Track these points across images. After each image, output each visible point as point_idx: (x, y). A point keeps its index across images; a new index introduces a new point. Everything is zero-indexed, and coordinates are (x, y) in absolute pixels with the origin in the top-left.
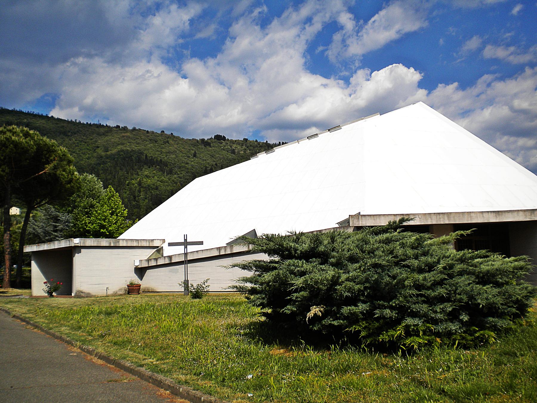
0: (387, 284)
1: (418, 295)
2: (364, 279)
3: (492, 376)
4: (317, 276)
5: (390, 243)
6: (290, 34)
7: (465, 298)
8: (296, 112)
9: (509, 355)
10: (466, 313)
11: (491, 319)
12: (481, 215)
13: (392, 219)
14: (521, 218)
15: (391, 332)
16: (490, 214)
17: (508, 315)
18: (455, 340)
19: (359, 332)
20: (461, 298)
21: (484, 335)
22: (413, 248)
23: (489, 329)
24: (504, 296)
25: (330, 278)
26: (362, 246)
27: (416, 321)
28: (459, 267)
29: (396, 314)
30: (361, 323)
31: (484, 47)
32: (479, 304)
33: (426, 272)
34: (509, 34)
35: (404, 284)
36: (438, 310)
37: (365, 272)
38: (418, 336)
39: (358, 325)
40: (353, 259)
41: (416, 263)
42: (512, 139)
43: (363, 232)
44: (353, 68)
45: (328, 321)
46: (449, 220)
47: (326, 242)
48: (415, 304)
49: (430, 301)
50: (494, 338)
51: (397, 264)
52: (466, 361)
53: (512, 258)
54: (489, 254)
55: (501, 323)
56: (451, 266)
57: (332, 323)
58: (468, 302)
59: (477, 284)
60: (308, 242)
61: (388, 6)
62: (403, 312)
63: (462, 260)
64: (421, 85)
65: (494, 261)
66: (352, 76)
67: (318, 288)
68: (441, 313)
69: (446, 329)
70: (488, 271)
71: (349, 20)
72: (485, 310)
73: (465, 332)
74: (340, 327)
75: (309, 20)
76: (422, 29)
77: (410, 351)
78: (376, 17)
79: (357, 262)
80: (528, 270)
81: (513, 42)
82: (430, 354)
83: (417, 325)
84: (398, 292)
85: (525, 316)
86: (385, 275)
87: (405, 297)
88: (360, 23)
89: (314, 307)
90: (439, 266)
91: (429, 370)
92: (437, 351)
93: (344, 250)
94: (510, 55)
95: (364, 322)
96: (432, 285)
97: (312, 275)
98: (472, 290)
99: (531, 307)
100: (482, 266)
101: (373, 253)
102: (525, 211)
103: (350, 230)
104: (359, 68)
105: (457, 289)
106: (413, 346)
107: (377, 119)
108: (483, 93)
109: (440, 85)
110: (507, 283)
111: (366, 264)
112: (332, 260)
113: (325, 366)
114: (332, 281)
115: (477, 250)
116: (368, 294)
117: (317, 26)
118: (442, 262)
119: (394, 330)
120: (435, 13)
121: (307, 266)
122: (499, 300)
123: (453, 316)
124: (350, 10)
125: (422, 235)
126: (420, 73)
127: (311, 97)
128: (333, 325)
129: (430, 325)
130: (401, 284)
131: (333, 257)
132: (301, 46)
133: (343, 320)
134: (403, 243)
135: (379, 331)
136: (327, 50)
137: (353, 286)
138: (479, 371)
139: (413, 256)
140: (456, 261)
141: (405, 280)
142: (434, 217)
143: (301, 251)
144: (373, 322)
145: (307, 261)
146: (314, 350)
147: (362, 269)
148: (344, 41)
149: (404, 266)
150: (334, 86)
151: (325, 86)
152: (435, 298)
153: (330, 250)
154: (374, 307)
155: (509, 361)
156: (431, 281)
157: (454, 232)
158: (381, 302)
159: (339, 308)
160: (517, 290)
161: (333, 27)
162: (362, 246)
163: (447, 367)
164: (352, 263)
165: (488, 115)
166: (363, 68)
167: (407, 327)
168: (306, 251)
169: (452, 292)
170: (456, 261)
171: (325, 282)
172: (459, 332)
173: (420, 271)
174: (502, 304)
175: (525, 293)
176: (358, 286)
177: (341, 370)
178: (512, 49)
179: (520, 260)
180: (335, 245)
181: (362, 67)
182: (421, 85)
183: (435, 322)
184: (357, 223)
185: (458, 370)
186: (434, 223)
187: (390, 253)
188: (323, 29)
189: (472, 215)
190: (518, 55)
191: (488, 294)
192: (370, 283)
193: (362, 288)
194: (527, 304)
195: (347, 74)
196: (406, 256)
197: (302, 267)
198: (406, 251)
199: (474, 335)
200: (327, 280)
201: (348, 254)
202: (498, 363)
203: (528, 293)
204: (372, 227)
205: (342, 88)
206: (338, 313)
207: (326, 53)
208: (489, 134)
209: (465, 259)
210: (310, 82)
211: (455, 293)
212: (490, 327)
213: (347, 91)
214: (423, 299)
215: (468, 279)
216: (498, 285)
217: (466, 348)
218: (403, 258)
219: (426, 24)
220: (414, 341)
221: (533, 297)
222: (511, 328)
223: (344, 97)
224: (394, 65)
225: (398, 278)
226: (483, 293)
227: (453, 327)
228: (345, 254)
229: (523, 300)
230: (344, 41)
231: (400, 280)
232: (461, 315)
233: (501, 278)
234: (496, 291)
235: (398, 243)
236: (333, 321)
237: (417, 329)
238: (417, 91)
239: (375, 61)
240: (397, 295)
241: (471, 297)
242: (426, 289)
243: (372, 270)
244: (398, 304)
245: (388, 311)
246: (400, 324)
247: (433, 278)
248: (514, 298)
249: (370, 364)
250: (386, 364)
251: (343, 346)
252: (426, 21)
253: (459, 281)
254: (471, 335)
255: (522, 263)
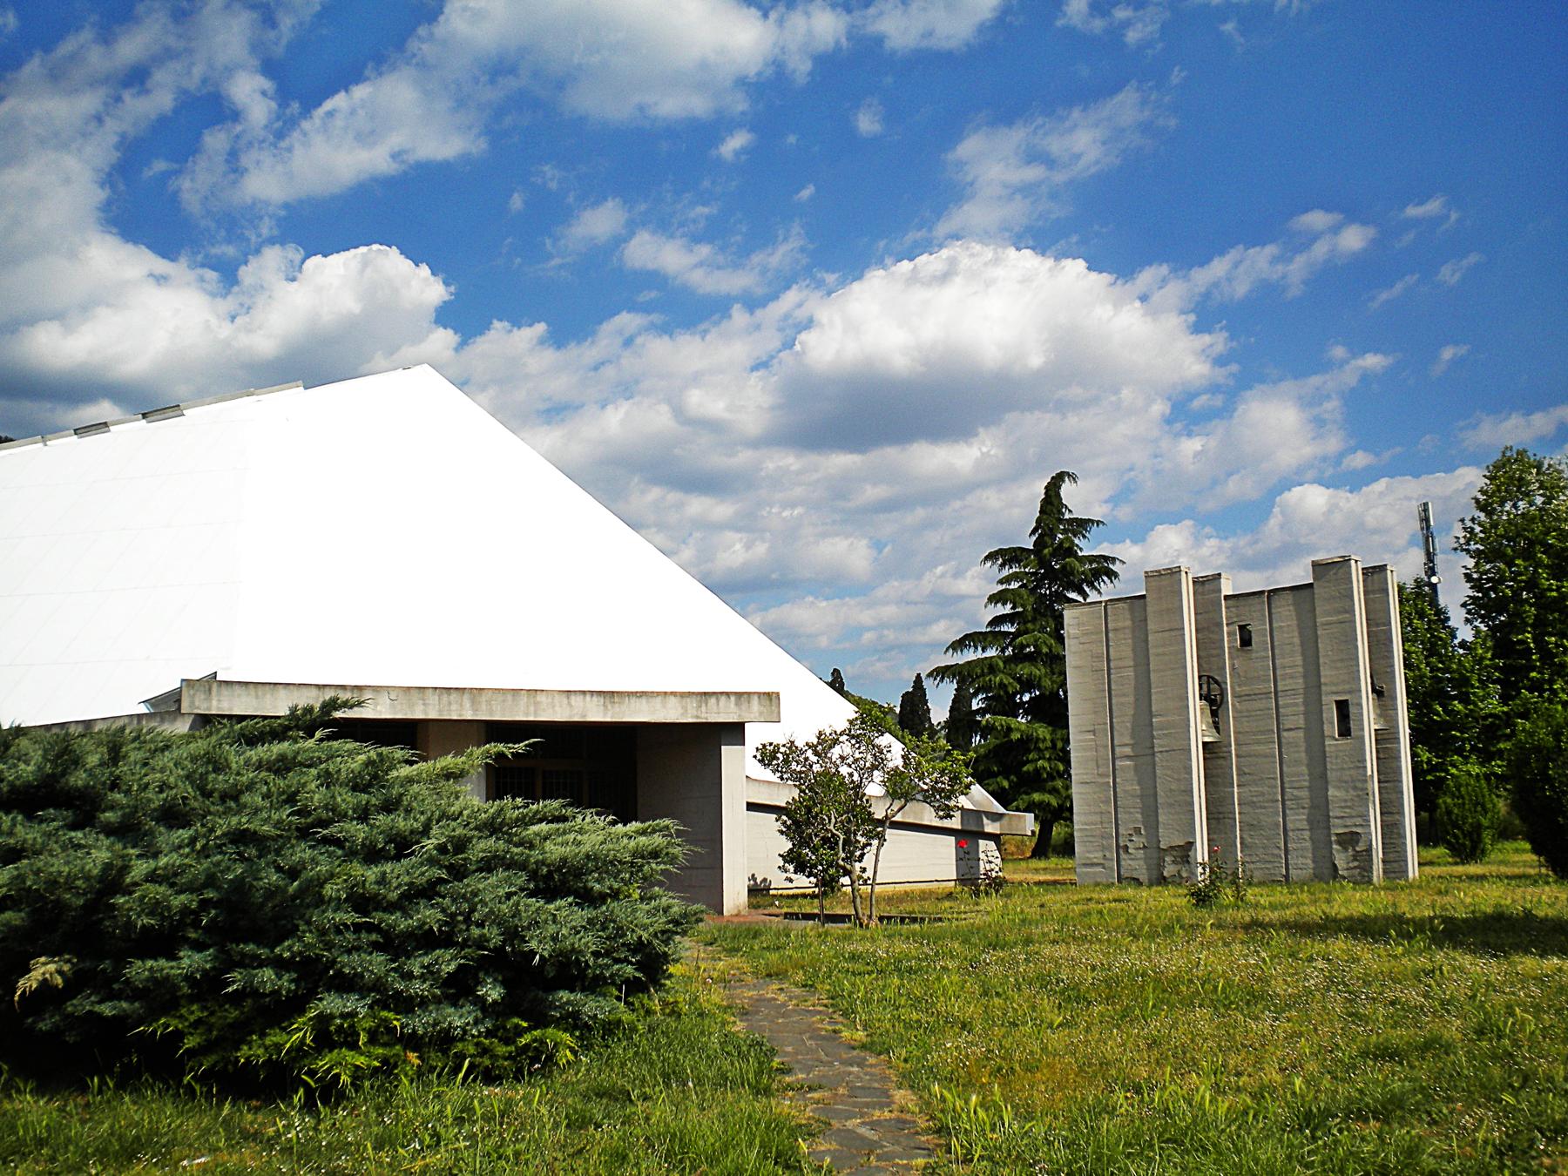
0: (271, 893)
1: (358, 928)
2: (202, 878)
3: (556, 1159)
4: (58, 865)
5: (289, 770)
6: (64, 108)
7: (494, 936)
8: (57, 347)
9: (610, 1097)
10: (495, 980)
11: (564, 995)
12: (565, 701)
13: (304, 700)
14: (596, 713)
15: (274, 1037)
16: (588, 697)
17: (613, 983)
18: (461, 1057)
19: (178, 1036)
20: (483, 935)
21: (542, 1042)
22: (356, 788)
23: (558, 1023)
24: (603, 930)
25: (95, 872)
26: (203, 776)
27: (351, 1003)
28: (483, 846)
29: (291, 981)
30: (183, 1011)
31: (632, 234)
32: (533, 953)
33: (388, 859)
34: (706, 210)
35: (320, 894)
36: (417, 971)
37: (207, 857)
38: (353, 1046)
39: (175, 1017)
40: (173, 816)
41: (358, 832)
42: (673, 496)
43: (211, 734)
44: (253, 238)
45: (82, 1004)
46: (475, 711)
47: (93, 760)
48: (349, 952)
49: (395, 946)
50: (572, 1050)
51: (304, 833)
52: (488, 1118)
53: (634, 826)
54: (569, 811)
55: (593, 1007)
56: (461, 845)
57: (97, 1008)
58: (503, 947)
59: (530, 896)
60: (37, 756)
61: (380, 74)
62: (315, 975)
63: (493, 827)
64: (444, 316)
65: (581, 831)
66: (246, 263)
67: (58, 901)
68: (423, 978)
69: (435, 1024)
70: (564, 860)
71: (258, 97)
72: (551, 972)
73: (490, 1034)
74: (121, 1022)
75: (137, 78)
76: (465, 158)
77: (329, 1093)
78: (339, 101)
79: (186, 824)
80: (673, 859)
81: (711, 233)
82: (387, 1101)
83: (353, 1014)
84: (302, 917)
85: (660, 987)
86: (268, 865)
87: (323, 932)
88: (288, 111)
89: (43, 959)
90: (426, 842)
91: (378, 1147)
92: (406, 1089)
93: (147, 785)
94: (696, 266)
95: (195, 1007)
96: (403, 896)
97: (39, 863)
98: (516, 914)
99: (677, 961)
100: (548, 845)
101: (236, 798)
102: (683, 695)
103: (182, 727)
104: (272, 241)
105: (473, 910)
106: (338, 1076)
107: (293, 398)
108: (610, 362)
109: (496, 324)
110: (615, 895)
111: (212, 830)
112: (109, 816)
113: (69, 1140)
114: (102, 878)
115: (536, 800)
116: (212, 920)
117: (160, 100)
118: (435, 830)
119: (284, 1029)
120: (508, 121)
121: (28, 833)
122: (588, 942)
123: (459, 988)
124: (269, 68)
125: (385, 750)
126: (446, 283)
127: (108, 305)
128: (99, 1016)
129: (391, 1015)
130: (312, 894)
131: (112, 808)
132: (101, 150)
133: (129, 999)
134: (328, 773)
135: (238, 1034)
136: (178, 172)
137: (166, 899)
138: (522, 1146)
139: (354, 811)
140: (476, 828)
141: (325, 881)
142: (433, 699)
143: (11, 784)
144: (221, 1006)
145: (30, 817)
146: (39, 1092)
147: (198, 846)
148: (233, 156)
149: (327, 841)
150: (189, 284)
151: (160, 279)
152: (409, 935)
153: (104, 783)
154: (228, 963)
155: (608, 1116)
156: (400, 885)
157: (479, 746)
158: (250, 948)
159: (121, 961)
160: (640, 916)
161: (211, 108)
162: (203, 776)
163: (432, 1137)
164: (170, 827)
165: (616, 423)
166: (283, 244)
167: (323, 1020)
168: (28, 786)
169: (460, 918)
170: (476, 828)
171: (79, 883)
172: (474, 1032)
173: (372, 855)
174: (596, 954)
175: (661, 922)
176: (183, 897)
177: (116, 1155)
178: (704, 250)
179: (654, 831)
180: (123, 768)
181: (280, 240)
182: (444, 316)
183: (406, 1004)
184: (205, 705)
185: (462, 1144)
186: (433, 715)
187: (286, 802)
188: (176, 111)
189: (541, 698)
190: (719, 268)
191: (561, 926)
192: (218, 889)
193: (194, 905)
194: (665, 953)
195: (230, 251)
196: (333, 810)
197: (11, 834)
198: (333, 797)
199: (514, 1042)
200: (87, 878)
201: (157, 800)
202: (579, 1123)
203: (669, 922)
204: (241, 718)
205: (213, 295)
206: (117, 981)
207: (173, 184)
208: (610, 478)
209: (502, 824)
210: (111, 260)
211: (468, 920)
212: (562, 1017)
213: (229, 304)
214: (374, 937)
215: (507, 880)
216: (588, 898)
217: (490, 1078)
218: (324, 815)
219: (476, 146)
220: (342, 1063)
221: (684, 933)
222: (619, 1021)
223: (214, 321)
224: (375, 247)
225: (303, 876)
226: (546, 921)
227: (457, 1018)
228: (149, 800)
229: (656, 942)
230: (233, 156)
231: (311, 880)
232: (482, 983)
233: (598, 881)
234: (581, 915)
235: (314, 771)
236: (100, 1002)
237: (352, 1026)
238: (430, 331)
239: (322, 226)
240: (296, 927)
241: (513, 934)
242: (385, 910)
243: (231, 849)
244: (300, 953)
245: (268, 974)
246: (302, 1012)
247: (407, 879)
248: (630, 938)
249: (206, 1132)
250: (256, 1133)
251: (128, 1082)
252: (482, 139)
253: (481, 886)
254: (507, 1041)
255: (658, 840)
